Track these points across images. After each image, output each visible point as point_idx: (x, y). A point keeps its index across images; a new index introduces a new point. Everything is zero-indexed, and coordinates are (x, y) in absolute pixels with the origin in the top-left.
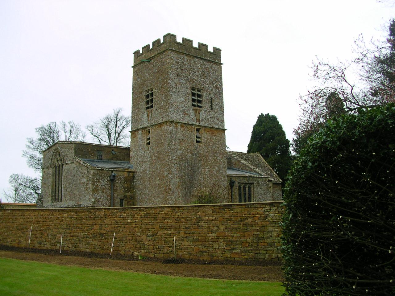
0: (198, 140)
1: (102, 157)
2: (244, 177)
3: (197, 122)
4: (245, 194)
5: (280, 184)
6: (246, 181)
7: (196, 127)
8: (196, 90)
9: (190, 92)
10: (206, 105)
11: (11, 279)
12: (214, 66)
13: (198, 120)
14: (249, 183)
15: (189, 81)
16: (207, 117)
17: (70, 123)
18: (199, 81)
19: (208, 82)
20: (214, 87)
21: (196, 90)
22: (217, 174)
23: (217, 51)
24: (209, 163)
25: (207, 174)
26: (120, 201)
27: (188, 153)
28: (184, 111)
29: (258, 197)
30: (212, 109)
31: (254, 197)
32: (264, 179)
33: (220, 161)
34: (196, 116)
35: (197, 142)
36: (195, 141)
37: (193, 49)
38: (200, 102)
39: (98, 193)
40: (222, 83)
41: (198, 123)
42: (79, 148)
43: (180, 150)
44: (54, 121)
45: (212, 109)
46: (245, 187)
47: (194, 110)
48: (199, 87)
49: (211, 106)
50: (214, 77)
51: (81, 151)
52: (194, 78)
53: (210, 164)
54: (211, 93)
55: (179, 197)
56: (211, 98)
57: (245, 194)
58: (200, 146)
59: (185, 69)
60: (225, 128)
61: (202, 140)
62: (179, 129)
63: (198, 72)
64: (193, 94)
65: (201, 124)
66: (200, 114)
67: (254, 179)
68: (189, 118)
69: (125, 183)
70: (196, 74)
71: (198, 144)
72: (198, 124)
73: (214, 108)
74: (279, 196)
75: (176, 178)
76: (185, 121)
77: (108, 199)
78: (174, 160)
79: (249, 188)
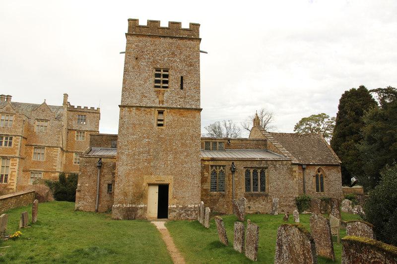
2: (253, 160)
3: (159, 104)
4: (255, 180)
5: (339, 165)
6: (255, 165)
8: (162, 71)
10: (174, 83)
12: (188, 42)
14: (261, 168)
20: (187, 65)
21: (162, 71)
23: (195, 27)
26: (108, 186)
27: (144, 137)
30: (182, 88)
31: (268, 184)
32: (285, 162)
35: (159, 125)
36: (155, 125)
37: (160, 30)
38: (166, 82)
40: (124, 77)
41: (161, 104)
43: (134, 135)
45: (182, 88)
46: (255, 173)
47: (155, 91)
48: (165, 67)
50: (187, 54)
55: (129, 186)
56: (182, 77)
57: (255, 180)
58: (162, 129)
60: (201, 108)
61: (166, 123)
63: (165, 51)
64: (157, 75)
65: (164, 106)
71: (160, 127)
72: (161, 105)
73: (184, 86)
75: (127, 165)
79: (263, 173)
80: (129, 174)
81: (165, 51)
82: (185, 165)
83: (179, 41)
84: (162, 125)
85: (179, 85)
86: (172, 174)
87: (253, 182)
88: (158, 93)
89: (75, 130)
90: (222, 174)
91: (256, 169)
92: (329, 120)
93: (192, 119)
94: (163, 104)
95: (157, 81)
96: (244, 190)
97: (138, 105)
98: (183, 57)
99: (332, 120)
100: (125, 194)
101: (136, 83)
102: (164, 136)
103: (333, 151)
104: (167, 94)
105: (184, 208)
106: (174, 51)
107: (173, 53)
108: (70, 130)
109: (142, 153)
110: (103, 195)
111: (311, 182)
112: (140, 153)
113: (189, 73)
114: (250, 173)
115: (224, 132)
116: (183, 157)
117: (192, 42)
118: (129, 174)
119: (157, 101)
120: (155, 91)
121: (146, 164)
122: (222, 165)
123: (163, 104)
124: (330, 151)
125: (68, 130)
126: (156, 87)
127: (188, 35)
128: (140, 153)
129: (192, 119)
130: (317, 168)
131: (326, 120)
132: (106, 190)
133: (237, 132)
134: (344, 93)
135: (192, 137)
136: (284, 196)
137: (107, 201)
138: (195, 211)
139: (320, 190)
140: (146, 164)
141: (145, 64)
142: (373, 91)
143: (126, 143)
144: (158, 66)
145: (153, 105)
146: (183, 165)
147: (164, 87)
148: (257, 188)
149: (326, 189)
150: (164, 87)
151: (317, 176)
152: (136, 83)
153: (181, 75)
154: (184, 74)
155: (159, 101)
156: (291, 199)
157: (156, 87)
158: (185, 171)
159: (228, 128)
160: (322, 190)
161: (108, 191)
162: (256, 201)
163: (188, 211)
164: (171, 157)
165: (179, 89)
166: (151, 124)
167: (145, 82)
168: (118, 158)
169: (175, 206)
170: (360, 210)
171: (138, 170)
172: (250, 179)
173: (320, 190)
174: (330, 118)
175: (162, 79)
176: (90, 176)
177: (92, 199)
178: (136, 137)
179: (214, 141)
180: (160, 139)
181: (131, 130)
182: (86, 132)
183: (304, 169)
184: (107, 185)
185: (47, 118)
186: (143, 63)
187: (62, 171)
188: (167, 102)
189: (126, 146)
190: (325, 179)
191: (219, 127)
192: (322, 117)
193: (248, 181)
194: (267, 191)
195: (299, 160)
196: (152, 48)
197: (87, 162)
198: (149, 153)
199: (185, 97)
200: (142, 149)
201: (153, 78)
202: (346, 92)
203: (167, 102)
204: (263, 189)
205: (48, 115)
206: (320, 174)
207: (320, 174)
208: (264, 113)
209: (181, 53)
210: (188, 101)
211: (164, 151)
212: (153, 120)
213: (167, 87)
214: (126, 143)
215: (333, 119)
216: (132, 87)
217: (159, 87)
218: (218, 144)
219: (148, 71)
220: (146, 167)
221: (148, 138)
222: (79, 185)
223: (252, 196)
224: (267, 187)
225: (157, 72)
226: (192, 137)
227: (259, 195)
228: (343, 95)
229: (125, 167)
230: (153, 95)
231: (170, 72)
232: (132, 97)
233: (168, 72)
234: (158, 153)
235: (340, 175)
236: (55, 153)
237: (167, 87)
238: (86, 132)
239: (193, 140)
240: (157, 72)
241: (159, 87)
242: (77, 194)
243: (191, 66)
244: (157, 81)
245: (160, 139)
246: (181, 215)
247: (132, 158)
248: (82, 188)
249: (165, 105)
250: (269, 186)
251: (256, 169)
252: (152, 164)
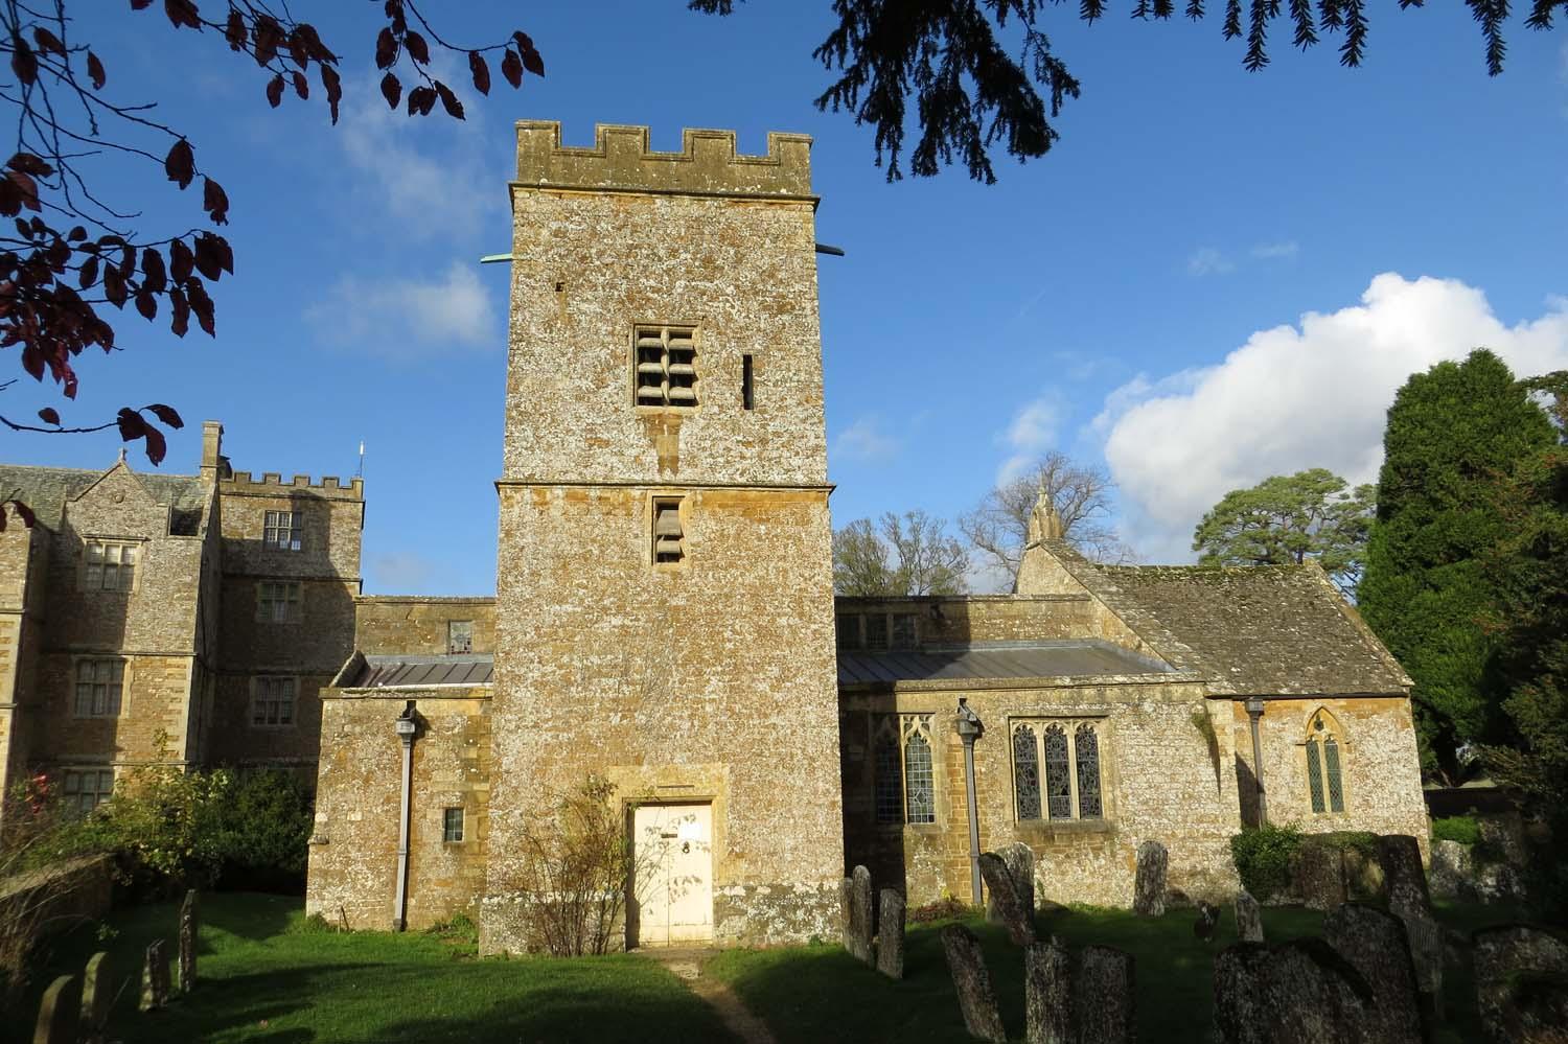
0: (665, 546)
1: (469, 643)
3: (660, 471)
4: (1057, 772)
7: (650, 494)
8: (664, 335)
9: (627, 349)
10: (715, 387)
11: (953, 953)
12: (768, 214)
13: (670, 462)
15: (623, 302)
16: (722, 445)
17: (910, 516)
18: (680, 290)
19: (730, 290)
22: (777, 696)
24: (729, 646)
25: (713, 696)
27: (605, 610)
28: (591, 430)
29: (1142, 779)
30: (748, 405)
33: (794, 632)
34: (653, 443)
35: (662, 557)
36: (647, 556)
38: (687, 380)
39: (345, 790)
42: (373, 620)
43: (562, 601)
44: (861, 518)
45: (748, 405)
47: (645, 419)
48: (677, 318)
49: (747, 391)
51: (383, 628)
52: (652, 282)
53: (733, 654)
54: (749, 333)
56: (748, 360)
57: (1057, 772)
58: (676, 575)
59: (600, 254)
62: (555, 513)
63: (673, 253)
65: (680, 478)
66: (677, 433)
67: (1109, 693)
68: (614, 459)
69: (468, 743)
70: (658, 268)
72: (668, 475)
73: (759, 394)
74: (1396, 756)
75: (536, 725)
76: (596, 472)
77: (387, 811)
78: (527, 646)
80: (546, 762)
81: (673, 253)
82: (773, 719)
83: (729, 212)
84: (675, 557)
85: (738, 390)
86: (723, 758)
87: (1050, 778)
88: (653, 426)
89: (257, 577)
90: (922, 749)
91: (1059, 724)
92: (1345, 497)
93: (792, 530)
94: (675, 471)
95: (646, 379)
96: (1009, 813)
97: (573, 477)
98: (747, 275)
99: (1358, 496)
100: (535, 848)
101: (563, 384)
102: (682, 603)
103: (1373, 637)
104: (691, 429)
105: (779, 893)
106: (711, 251)
107: (708, 261)
108: (234, 576)
109: (599, 674)
110: (424, 858)
111: (1286, 770)
112: (590, 675)
113: (776, 338)
114: (1033, 740)
115: (893, 562)
116: (763, 687)
117: (783, 214)
118: (546, 762)
119: (652, 457)
120: (645, 419)
121: (615, 719)
122: (920, 709)
123: (675, 471)
124: (1361, 636)
125: (225, 576)
126: (644, 401)
127: (767, 185)
128: (590, 675)
129: (792, 530)
130: (1311, 706)
131: (1331, 499)
132: (440, 837)
133: (946, 561)
134: (1404, 382)
135: (799, 602)
136: (1180, 833)
137: (444, 883)
138: (822, 907)
139: (1328, 806)
140: (615, 719)
141: (595, 307)
142: (1534, 384)
143: (531, 635)
144: (650, 316)
145: (638, 478)
146: (766, 716)
147: (675, 402)
148: (1067, 802)
149: (1351, 800)
150: (675, 402)
151: (1311, 747)
152: (563, 384)
153: (745, 351)
154: (756, 345)
155: (661, 461)
156: (1213, 845)
157: (644, 401)
158: (777, 742)
159: (909, 550)
160: (1338, 806)
161: (446, 837)
162: (1067, 856)
163: (796, 907)
164: (714, 685)
165: (737, 411)
166: (628, 554)
167: (601, 384)
168: (501, 698)
169: (740, 891)
170: (1508, 886)
171: (586, 743)
172: (1035, 766)
173: (1328, 806)
174: (1349, 490)
175: (663, 365)
176: (367, 780)
177: (379, 874)
178: (570, 608)
179: (874, 609)
180: (667, 617)
181: (547, 583)
182: (303, 586)
183: (1256, 715)
184: (440, 816)
185: (133, 532)
186: (586, 306)
187: (1214, 905)
188: (692, 462)
189: (531, 646)
190: (1344, 757)
191: (872, 545)
192: (1315, 484)
193: (1025, 775)
194: (1107, 813)
195: (1231, 678)
196: (622, 241)
197: (354, 721)
198: (625, 673)
199: (764, 442)
200: (595, 660)
201: (626, 373)
202: (1415, 380)
203: (692, 462)
204: (1092, 806)
205: (137, 517)
206: (1323, 734)
207: (1323, 734)
208: (1059, 475)
209: (739, 260)
210: (775, 454)
211: (687, 661)
212: (636, 536)
213: (690, 402)
214: (531, 635)
215: (1362, 492)
216: (545, 407)
217: (657, 401)
218: (890, 621)
219: (608, 339)
220: (618, 732)
221: (620, 610)
222: (320, 817)
223: (1050, 838)
224: (1106, 798)
225: (646, 341)
226: (799, 602)
227: (1074, 832)
228: (1401, 393)
229: (530, 736)
230: (634, 436)
231: (695, 342)
232: (551, 446)
233: (689, 336)
234: (664, 672)
235: (1410, 737)
236: (170, 683)
237: (691, 402)
238: (303, 586)
239: (801, 615)
240: (646, 341)
241: (657, 401)
242: (315, 859)
243: (781, 310)
244: (646, 379)
245: (667, 617)
246: (764, 925)
247: (557, 698)
248: (336, 831)
249: (686, 474)
250: (1118, 792)
251: (1059, 724)
252: (641, 719)
